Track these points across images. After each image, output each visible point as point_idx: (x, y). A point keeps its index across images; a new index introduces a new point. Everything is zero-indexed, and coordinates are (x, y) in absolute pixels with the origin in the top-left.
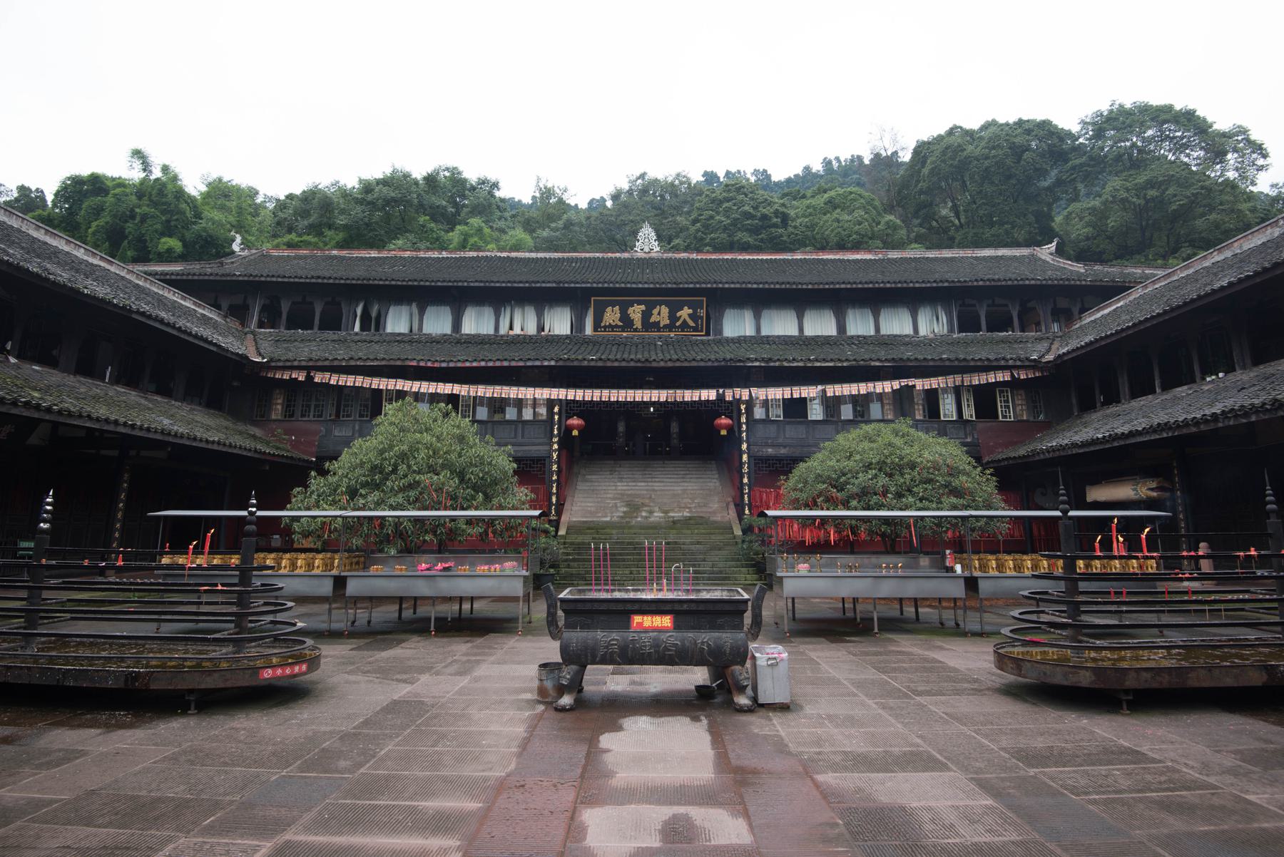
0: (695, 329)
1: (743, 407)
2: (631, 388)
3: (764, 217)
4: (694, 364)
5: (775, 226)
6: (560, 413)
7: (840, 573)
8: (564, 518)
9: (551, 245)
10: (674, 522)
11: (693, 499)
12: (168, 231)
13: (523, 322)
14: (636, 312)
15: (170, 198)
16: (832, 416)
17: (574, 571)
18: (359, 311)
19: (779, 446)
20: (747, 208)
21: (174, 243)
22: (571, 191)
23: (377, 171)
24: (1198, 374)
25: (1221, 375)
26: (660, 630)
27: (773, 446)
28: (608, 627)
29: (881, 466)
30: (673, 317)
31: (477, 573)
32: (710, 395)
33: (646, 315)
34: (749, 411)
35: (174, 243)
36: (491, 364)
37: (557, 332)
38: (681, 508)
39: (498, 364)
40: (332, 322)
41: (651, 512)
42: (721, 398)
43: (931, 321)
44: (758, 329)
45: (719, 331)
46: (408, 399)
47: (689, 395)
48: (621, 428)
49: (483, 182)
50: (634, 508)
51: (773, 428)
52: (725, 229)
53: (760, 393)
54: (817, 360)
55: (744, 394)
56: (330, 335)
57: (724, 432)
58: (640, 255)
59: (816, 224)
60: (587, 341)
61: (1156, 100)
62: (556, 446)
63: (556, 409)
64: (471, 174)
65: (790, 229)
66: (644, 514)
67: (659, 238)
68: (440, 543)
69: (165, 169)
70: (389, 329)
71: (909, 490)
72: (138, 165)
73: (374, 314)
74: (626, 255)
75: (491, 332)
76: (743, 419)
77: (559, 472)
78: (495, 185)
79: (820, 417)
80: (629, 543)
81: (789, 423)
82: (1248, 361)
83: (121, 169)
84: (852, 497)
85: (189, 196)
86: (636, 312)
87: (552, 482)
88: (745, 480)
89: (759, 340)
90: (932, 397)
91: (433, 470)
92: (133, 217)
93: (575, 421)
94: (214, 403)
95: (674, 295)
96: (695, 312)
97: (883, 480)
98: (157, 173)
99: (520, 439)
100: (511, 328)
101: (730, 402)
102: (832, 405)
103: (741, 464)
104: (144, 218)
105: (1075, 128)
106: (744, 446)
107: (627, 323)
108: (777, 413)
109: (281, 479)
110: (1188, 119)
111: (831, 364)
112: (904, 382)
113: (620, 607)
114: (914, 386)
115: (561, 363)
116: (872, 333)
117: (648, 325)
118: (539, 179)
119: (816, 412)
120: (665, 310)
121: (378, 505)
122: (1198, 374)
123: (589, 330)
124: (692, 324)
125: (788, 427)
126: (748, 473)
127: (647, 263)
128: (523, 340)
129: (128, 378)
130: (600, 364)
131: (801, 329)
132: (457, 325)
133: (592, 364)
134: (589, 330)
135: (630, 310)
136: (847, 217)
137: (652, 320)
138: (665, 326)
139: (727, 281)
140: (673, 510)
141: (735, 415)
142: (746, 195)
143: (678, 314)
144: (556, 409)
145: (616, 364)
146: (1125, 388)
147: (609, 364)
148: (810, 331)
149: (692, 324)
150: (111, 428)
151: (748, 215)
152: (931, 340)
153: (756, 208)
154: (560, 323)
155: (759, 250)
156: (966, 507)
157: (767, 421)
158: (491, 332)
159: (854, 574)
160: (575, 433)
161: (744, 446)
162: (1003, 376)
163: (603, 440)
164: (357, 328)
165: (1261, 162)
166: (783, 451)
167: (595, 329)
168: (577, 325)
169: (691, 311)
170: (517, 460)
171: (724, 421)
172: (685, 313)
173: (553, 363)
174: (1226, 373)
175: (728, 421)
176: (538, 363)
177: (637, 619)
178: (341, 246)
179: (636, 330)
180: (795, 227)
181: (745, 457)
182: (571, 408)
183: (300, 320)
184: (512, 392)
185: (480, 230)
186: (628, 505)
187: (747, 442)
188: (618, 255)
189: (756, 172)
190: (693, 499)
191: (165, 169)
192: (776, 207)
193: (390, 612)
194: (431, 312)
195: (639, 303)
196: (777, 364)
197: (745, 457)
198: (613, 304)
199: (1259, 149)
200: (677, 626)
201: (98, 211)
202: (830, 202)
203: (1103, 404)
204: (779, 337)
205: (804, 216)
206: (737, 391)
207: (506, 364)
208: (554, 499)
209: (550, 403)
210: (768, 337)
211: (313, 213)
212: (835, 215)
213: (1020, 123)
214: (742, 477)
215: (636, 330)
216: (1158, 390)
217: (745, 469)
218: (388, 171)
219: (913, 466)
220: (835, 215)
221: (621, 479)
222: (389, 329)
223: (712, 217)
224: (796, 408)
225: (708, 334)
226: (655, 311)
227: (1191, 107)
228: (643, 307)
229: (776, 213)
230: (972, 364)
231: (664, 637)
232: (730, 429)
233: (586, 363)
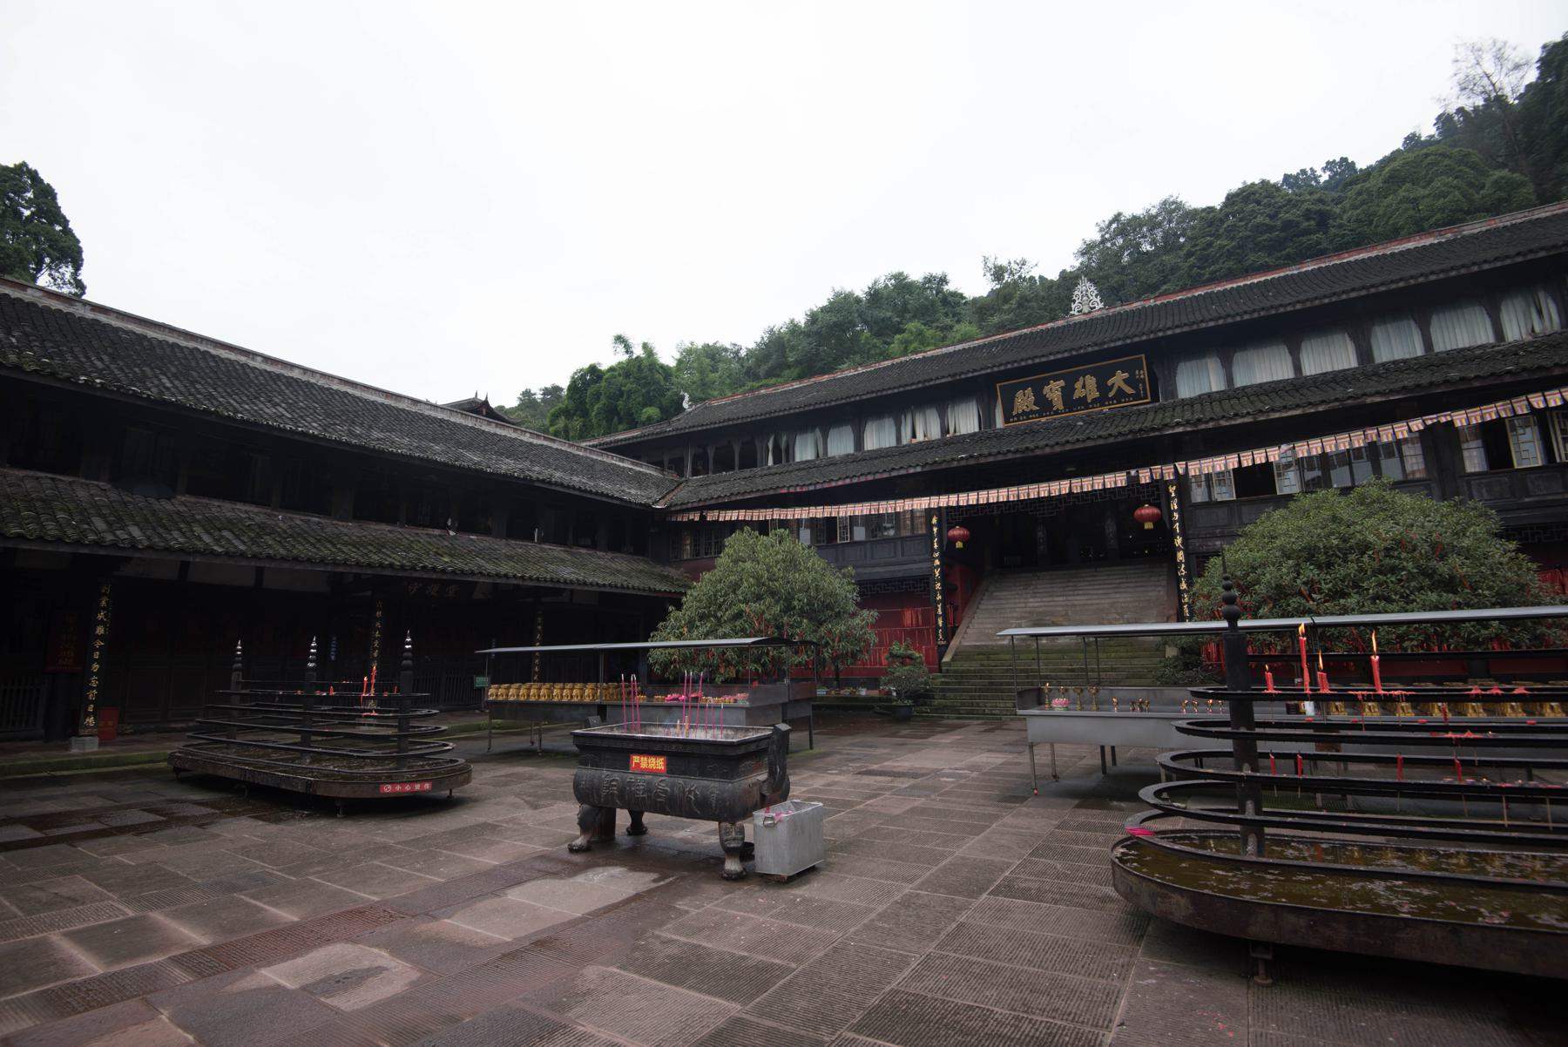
0: (1136, 397)
1: (1172, 489)
2: (973, 490)
3: (1288, 225)
4: (1090, 444)
5: (1307, 232)
6: (939, 525)
7: (1115, 712)
8: (954, 643)
9: (1002, 328)
12: (648, 402)
13: (926, 428)
14: (1054, 391)
15: (646, 372)
17: (948, 702)
18: (770, 446)
20: (1260, 219)
21: (651, 411)
22: (1031, 262)
23: (821, 300)
26: (654, 773)
28: (612, 766)
29: (1310, 554)
30: (1103, 387)
31: (655, 703)
32: (1116, 480)
33: (1067, 392)
35: (651, 411)
36: (855, 480)
37: (963, 431)
39: (863, 479)
40: (750, 461)
42: (1133, 481)
43: (1527, 316)
44: (1230, 380)
45: (1173, 393)
46: (747, 528)
49: (929, 280)
51: (1222, 513)
52: (1230, 254)
53: (1197, 468)
54: (1273, 410)
56: (747, 473)
57: (1148, 526)
58: (1078, 318)
59: (1374, 214)
60: (1000, 436)
62: (937, 562)
63: (934, 521)
64: (916, 275)
65: (1333, 231)
67: (1101, 293)
68: (766, 673)
69: (645, 346)
70: (798, 459)
71: (1356, 585)
72: (621, 348)
73: (783, 446)
74: (1060, 323)
75: (893, 443)
77: (943, 592)
78: (943, 280)
80: (1022, 671)
83: (609, 358)
84: (1264, 602)
85: (662, 366)
86: (1054, 391)
87: (937, 602)
89: (1232, 394)
90: (1495, 437)
91: (759, 598)
92: (621, 394)
93: (957, 532)
94: (639, 550)
95: (1100, 360)
96: (1132, 375)
97: (1310, 572)
98: (638, 352)
99: (900, 558)
100: (914, 436)
104: (630, 393)
106: (1179, 541)
107: (1044, 405)
108: (1226, 493)
109: (647, 612)
111: (1298, 412)
112: (1431, 420)
113: (619, 745)
114: (1452, 422)
115: (927, 468)
116: (1420, 352)
117: (1070, 403)
118: (986, 260)
120: (1091, 381)
121: (706, 636)
123: (1000, 423)
124: (1129, 390)
125: (1245, 509)
127: (1090, 325)
128: (928, 446)
129: (558, 537)
130: (972, 462)
131: (1298, 368)
132: (859, 443)
133: (963, 463)
134: (1000, 423)
135: (1046, 389)
136: (1422, 192)
137: (1076, 395)
138: (1095, 401)
139: (1171, 327)
142: (1258, 203)
143: (1110, 382)
144: (934, 521)
145: (991, 459)
147: (982, 460)
148: (1311, 367)
149: (1129, 390)
150: (503, 581)
151: (1260, 229)
152: (1530, 344)
154: (966, 421)
155: (1277, 268)
156: (1459, 606)
157: (1211, 504)
158: (893, 443)
159: (1138, 713)
160: (959, 545)
161: (1179, 541)
163: (1001, 550)
164: (770, 463)
167: (1007, 421)
168: (986, 419)
169: (1126, 375)
170: (859, 583)
171: (1147, 510)
172: (1118, 379)
173: (919, 469)
176: (903, 472)
177: (636, 759)
178: (800, 377)
179: (1057, 413)
180: (1340, 226)
181: (1180, 556)
182: (950, 516)
183: (724, 464)
184: (886, 507)
185: (920, 333)
187: (1183, 534)
188: (1050, 325)
189: (1330, 165)
191: (645, 346)
192: (1306, 206)
194: (834, 435)
195: (1056, 379)
196: (1211, 425)
197: (1180, 556)
198: (1024, 387)
200: (671, 770)
201: (597, 396)
202: (1391, 177)
204: (1261, 385)
205: (1354, 207)
207: (870, 478)
208: (940, 622)
209: (929, 512)
210: (1244, 388)
211: (778, 353)
212: (1402, 193)
214: (1179, 582)
215: (1057, 413)
218: (830, 295)
219: (1364, 547)
220: (1402, 193)
221: (1035, 595)
222: (798, 459)
223: (1210, 244)
224: (1256, 483)
225: (1155, 399)
226: (1078, 385)
228: (1062, 383)
229: (1307, 215)
230: (1557, 372)
231: (657, 780)
233: (955, 464)
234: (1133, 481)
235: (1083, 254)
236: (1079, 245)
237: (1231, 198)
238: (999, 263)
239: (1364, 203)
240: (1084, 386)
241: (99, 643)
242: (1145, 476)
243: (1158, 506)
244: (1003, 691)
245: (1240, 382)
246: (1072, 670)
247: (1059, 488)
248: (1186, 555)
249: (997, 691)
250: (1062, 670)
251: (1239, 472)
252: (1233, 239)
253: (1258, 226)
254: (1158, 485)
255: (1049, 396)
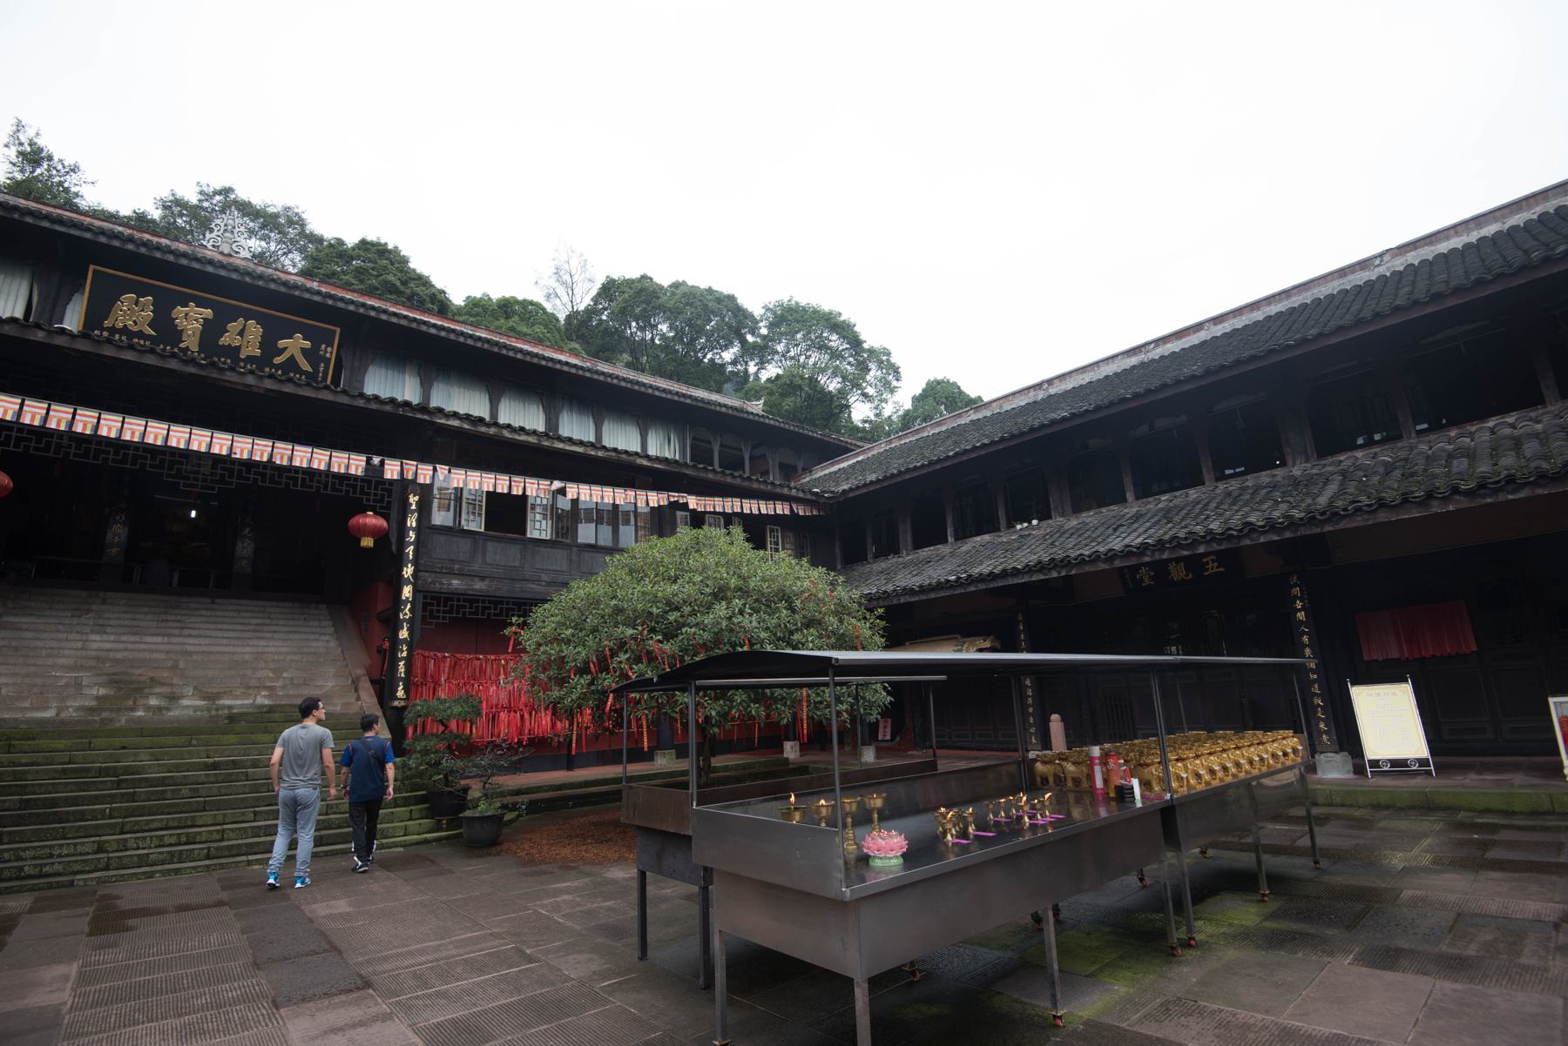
1: (413, 499)
10: (232, 718)
11: (278, 672)
16: (565, 535)
19: (472, 576)
20: (391, 278)
24: (1003, 522)
25: (1035, 522)
27: (460, 575)
32: (352, 464)
34: (424, 509)
38: (248, 688)
41: (173, 698)
42: (374, 473)
47: (303, 456)
48: (118, 533)
50: (127, 687)
51: (465, 545)
55: (424, 473)
57: (367, 542)
61: (826, 307)
66: (153, 702)
76: (412, 522)
79: (546, 535)
81: (493, 539)
82: (1068, 507)
88: (404, 634)
96: (316, 347)
101: (391, 482)
102: (566, 521)
103: (397, 602)
105: (756, 309)
106: (408, 571)
110: (845, 330)
112: (675, 497)
118: (19, 126)
119: (538, 528)
120: (255, 330)
122: (1003, 522)
124: (305, 366)
125: (490, 546)
126: (411, 621)
135: (180, 311)
137: (225, 340)
138: (250, 359)
140: (228, 694)
141: (394, 514)
143: (282, 343)
146: (906, 538)
149: (305, 366)
153: (404, 283)
157: (456, 531)
161: (408, 571)
162: (781, 509)
165: (895, 383)
166: (479, 585)
171: (371, 520)
172: (295, 345)
174: (1040, 520)
175: (380, 522)
181: (407, 592)
186: (114, 681)
187: (416, 563)
190: (278, 672)
193: (96, 742)
195: (201, 303)
197: (407, 592)
198: (141, 291)
199: (896, 371)
203: (876, 557)
206: (411, 466)
213: (710, 290)
216: (950, 539)
217: (406, 613)
221: (101, 629)
224: (506, 514)
226: (234, 326)
227: (852, 321)
228: (208, 313)
232: (381, 537)
234: (374, 473)
235: (165, 207)
236: (165, 194)
237: (364, 244)
238: (41, 142)
239: (478, 315)
240: (241, 333)
241: (1033, 730)
242: (392, 470)
243: (386, 517)
244: (60, 818)
245: (435, 403)
246: (215, 766)
247: (246, 447)
248: (415, 591)
249: (44, 819)
250: (195, 767)
251: (492, 496)
252: (361, 281)
253: (386, 282)
254: (405, 485)
255: (180, 323)
